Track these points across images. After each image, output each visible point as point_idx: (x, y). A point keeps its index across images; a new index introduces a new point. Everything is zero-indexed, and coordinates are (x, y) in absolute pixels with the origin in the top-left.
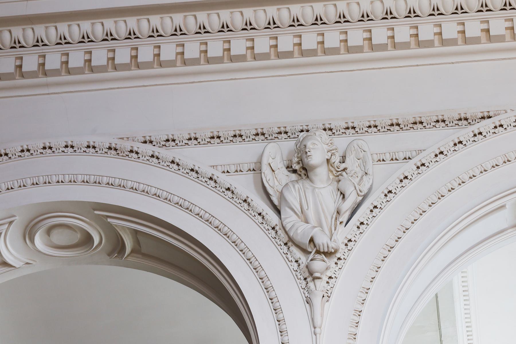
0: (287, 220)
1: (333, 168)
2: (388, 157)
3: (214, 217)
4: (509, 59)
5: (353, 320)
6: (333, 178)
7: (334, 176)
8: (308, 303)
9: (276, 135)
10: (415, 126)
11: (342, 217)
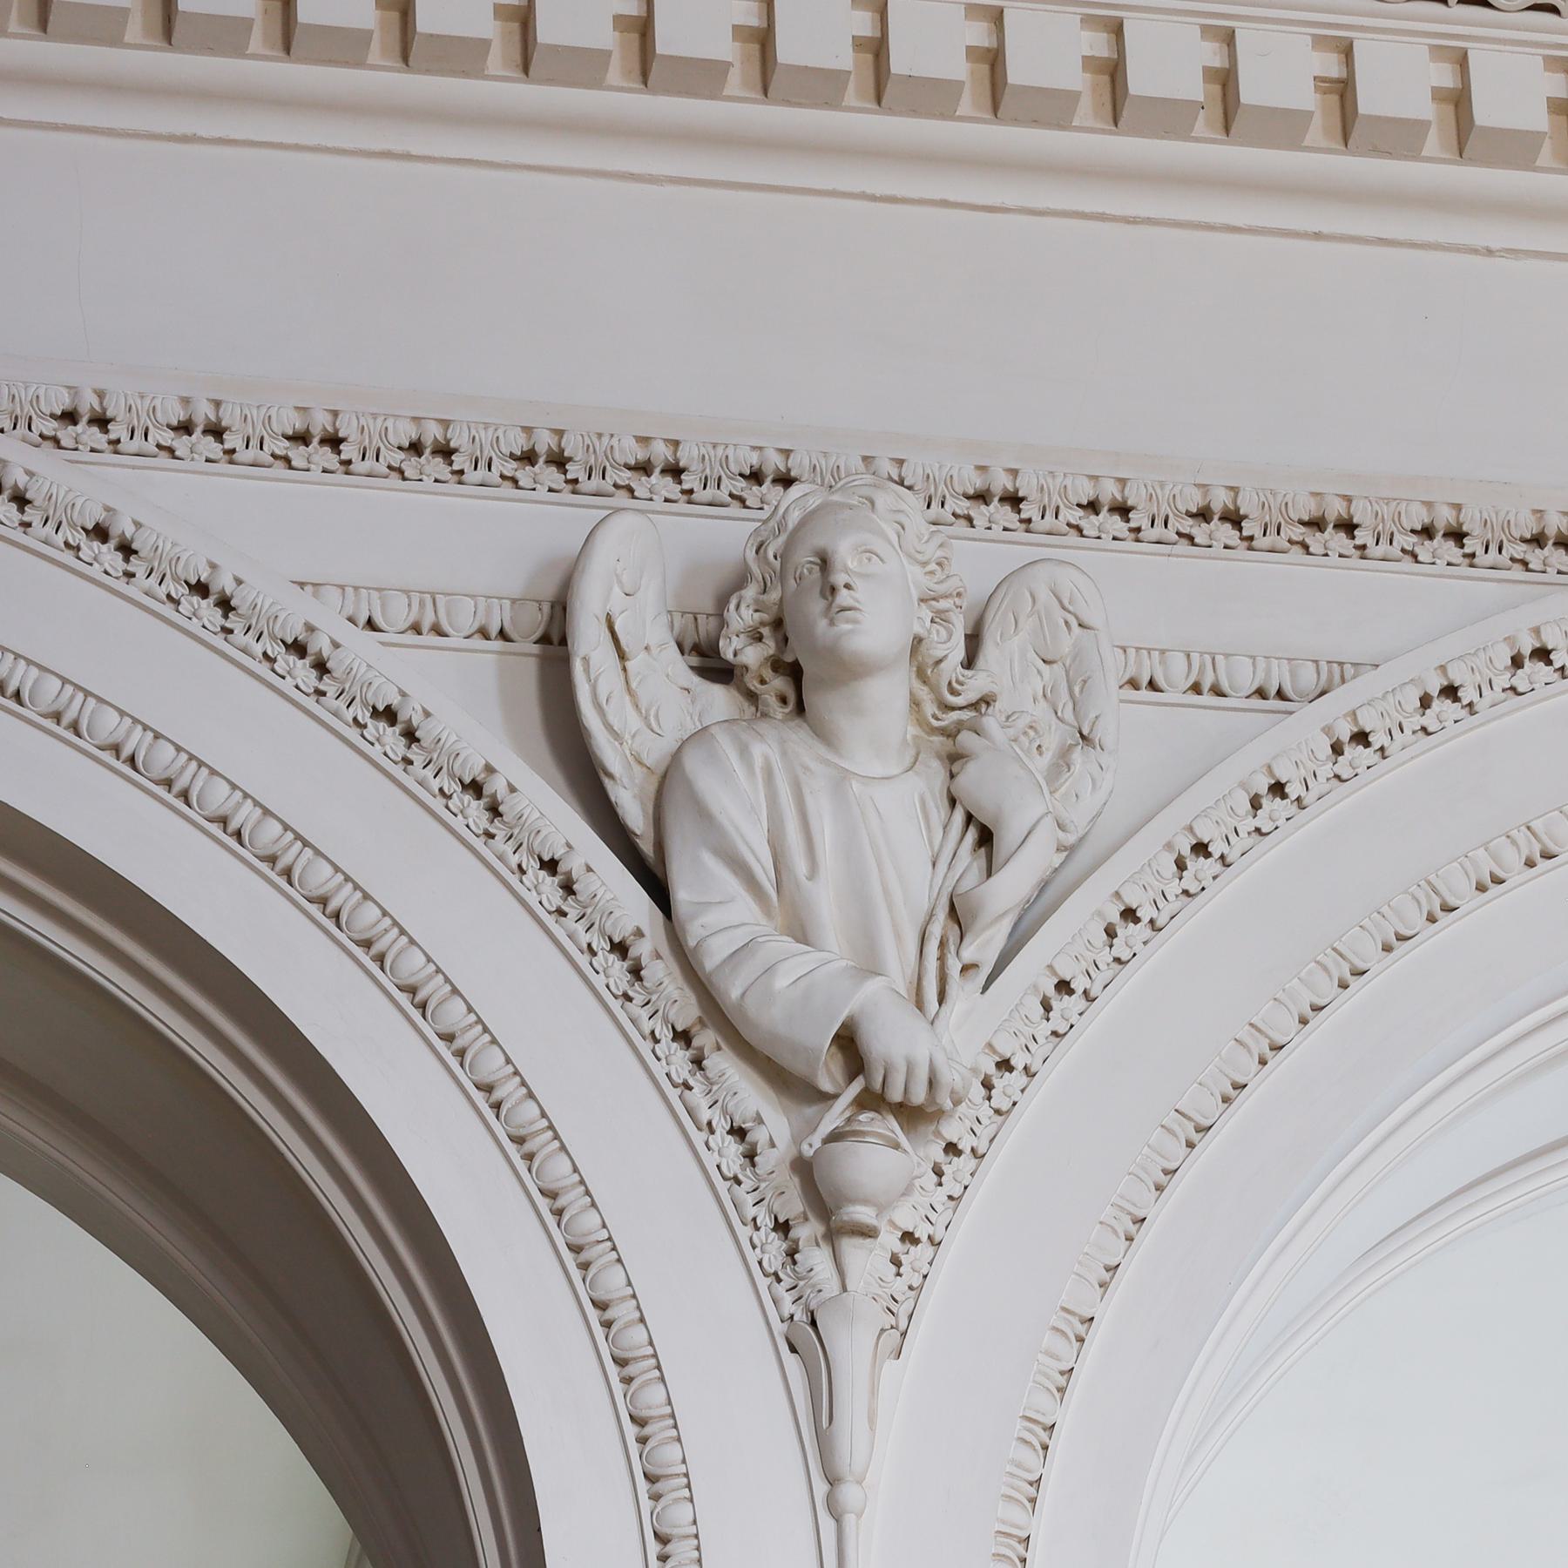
0: (712, 919)
1: (926, 689)
2: (1177, 673)
3: (306, 844)
4: (1127, 221)
5: (1019, 1465)
6: (915, 737)
7: (918, 728)
8: (793, 1349)
9: (625, 477)
10: (1315, 540)
11: (974, 941)
